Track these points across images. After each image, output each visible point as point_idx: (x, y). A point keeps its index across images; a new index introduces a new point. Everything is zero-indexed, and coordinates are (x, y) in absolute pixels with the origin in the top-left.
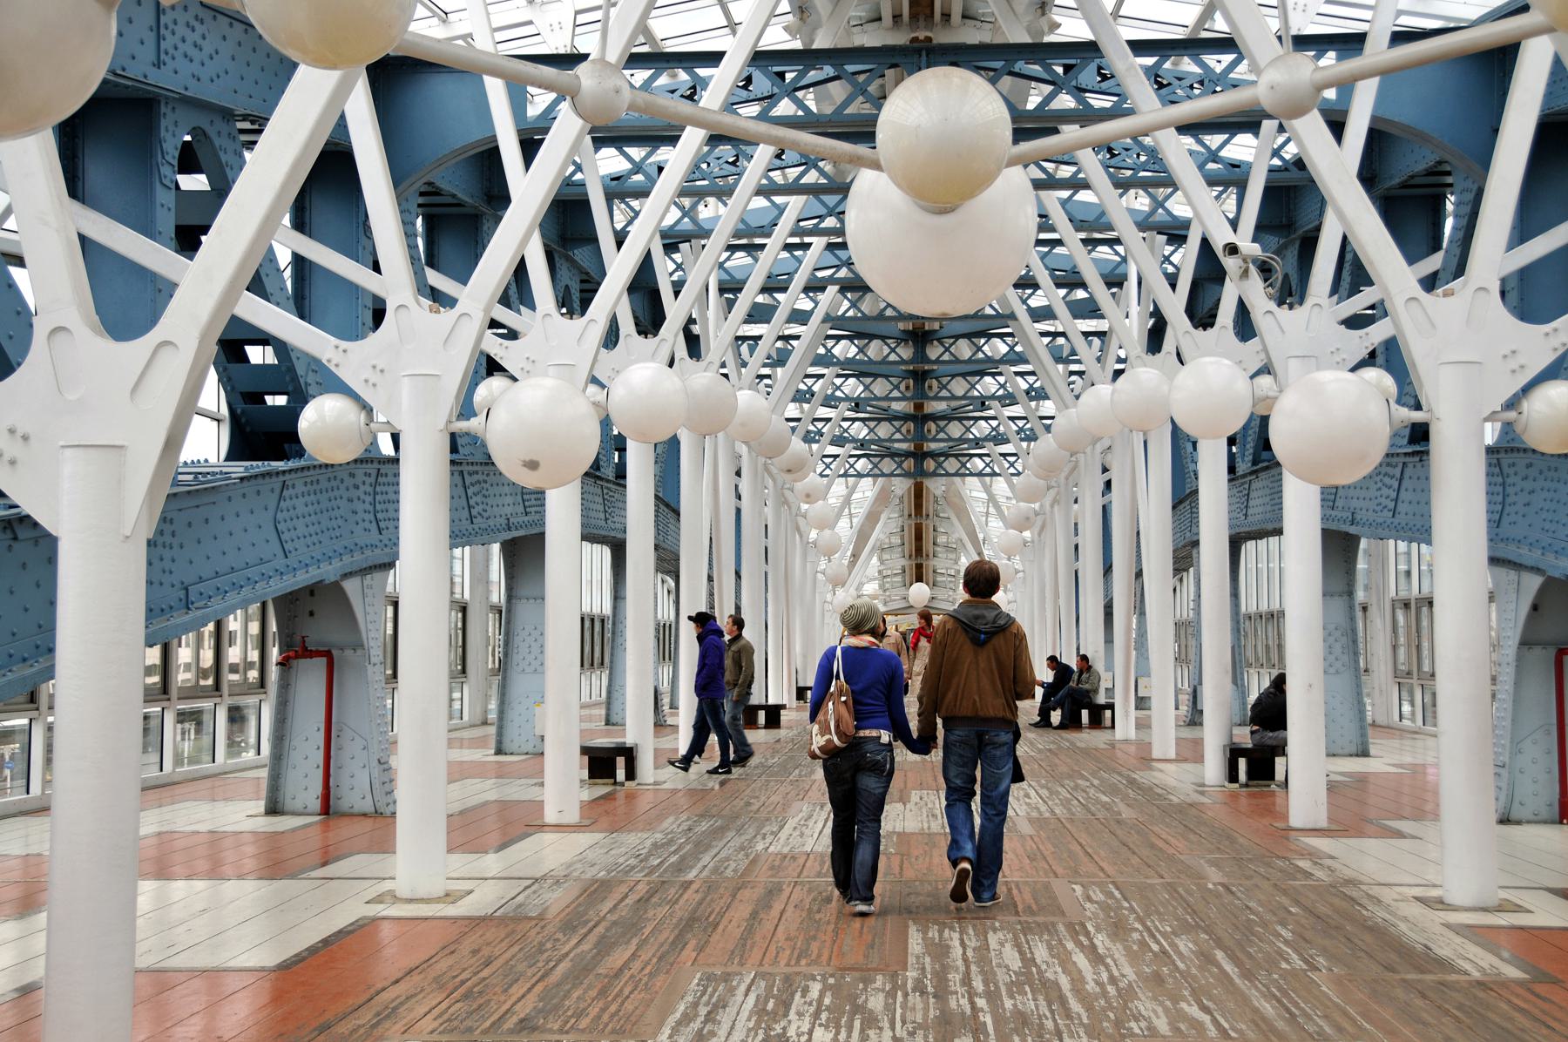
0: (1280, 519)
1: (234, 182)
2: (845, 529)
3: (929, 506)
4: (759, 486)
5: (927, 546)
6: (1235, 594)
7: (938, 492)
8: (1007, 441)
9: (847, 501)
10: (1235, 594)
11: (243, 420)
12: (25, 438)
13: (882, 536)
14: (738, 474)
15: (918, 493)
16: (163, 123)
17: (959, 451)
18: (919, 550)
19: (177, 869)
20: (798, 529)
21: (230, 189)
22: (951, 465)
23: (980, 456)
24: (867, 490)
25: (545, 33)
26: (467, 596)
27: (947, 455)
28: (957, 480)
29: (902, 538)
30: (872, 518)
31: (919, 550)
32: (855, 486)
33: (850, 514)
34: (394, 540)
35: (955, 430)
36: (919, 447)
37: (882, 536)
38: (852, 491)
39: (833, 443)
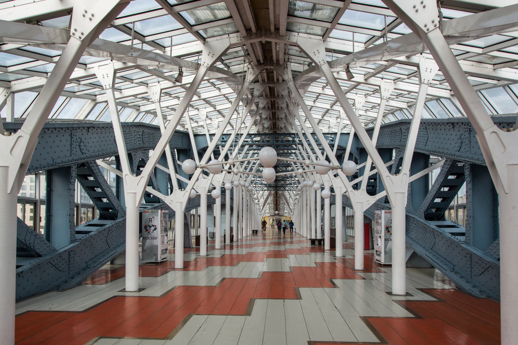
0: (335, 202)
1: (147, 163)
2: (262, 201)
3: (278, 195)
4: (247, 194)
5: (278, 203)
6: (330, 214)
7: (280, 193)
8: (292, 185)
9: (263, 195)
10: (330, 214)
11: (103, 215)
12: (424, 7)
13: (269, 201)
14: (243, 191)
15: (276, 193)
16: (134, 162)
17: (284, 187)
18: (277, 204)
19: (373, 270)
20: (253, 201)
21: (146, 164)
22: (282, 189)
23: (288, 187)
24: (266, 193)
25: (213, 125)
26: (194, 213)
27: (281, 187)
28: (284, 191)
29: (273, 201)
30: (267, 198)
31: (277, 204)
32: (264, 192)
33: (263, 197)
34: (421, 125)
35: (282, 182)
36: (276, 185)
37: (269, 201)
38: (264, 193)
39: (260, 185)
